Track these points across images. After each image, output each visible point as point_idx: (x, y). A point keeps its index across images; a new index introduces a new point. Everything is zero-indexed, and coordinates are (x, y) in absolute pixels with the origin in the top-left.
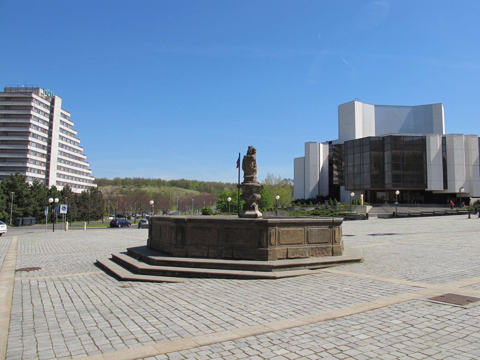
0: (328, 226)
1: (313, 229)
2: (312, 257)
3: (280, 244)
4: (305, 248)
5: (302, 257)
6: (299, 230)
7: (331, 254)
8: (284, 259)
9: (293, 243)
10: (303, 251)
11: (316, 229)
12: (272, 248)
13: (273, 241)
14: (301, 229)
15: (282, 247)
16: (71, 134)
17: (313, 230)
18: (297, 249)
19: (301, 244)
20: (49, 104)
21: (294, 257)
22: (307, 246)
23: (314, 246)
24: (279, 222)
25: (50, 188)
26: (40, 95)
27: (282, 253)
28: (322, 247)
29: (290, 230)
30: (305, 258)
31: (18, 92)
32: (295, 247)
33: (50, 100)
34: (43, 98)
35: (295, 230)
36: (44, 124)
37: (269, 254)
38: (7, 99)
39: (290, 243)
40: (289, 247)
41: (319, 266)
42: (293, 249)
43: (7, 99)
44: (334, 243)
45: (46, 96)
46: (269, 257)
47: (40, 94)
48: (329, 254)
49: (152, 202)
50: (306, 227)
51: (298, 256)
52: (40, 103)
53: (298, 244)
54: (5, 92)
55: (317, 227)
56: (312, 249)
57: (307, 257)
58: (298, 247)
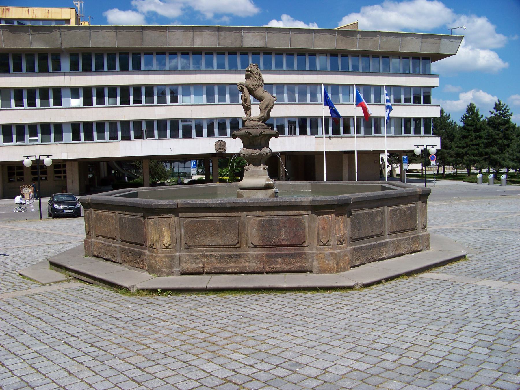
22: (120, 244)
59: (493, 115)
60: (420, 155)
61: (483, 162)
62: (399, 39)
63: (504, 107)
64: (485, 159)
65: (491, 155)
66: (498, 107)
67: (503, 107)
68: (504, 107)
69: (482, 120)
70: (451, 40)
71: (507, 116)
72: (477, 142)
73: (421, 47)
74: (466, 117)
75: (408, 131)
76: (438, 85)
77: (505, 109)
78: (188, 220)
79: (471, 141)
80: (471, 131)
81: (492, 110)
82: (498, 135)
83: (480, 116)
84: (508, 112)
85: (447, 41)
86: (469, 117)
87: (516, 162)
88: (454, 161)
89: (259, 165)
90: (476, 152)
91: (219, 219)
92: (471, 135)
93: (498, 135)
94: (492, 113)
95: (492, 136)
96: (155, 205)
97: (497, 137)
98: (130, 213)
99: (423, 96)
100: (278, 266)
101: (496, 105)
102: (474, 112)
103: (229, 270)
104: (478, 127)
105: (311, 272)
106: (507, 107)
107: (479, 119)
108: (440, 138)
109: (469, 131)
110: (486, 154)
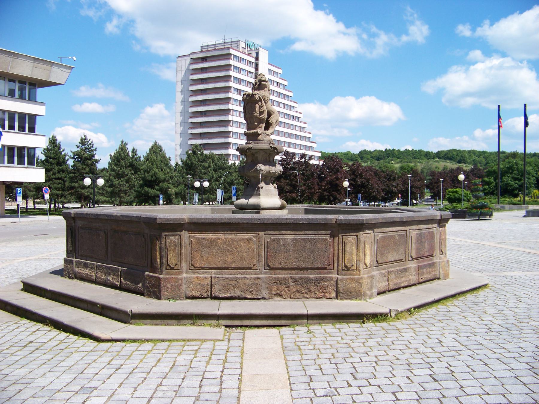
0: (329, 232)
1: (281, 237)
2: (277, 298)
3: (195, 268)
4: (259, 278)
5: (249, 297)
6: (243, 239)
7: (334, 294)
8: (202, 298)
9: (226, 266)
10: (254, 284)
11: (292, 237)
12: (172, 274)
13: (172, 259)
14: (247, 237)
15: (198, 273)
16: (285, 96)
17: (281, 242)
18: (235, 279)
19: (250, 268)
20: (253, 60)
21: (228, 295)
22: (266, 273)
23: (283, 275)
24: (187, 221)
25: (71, 163)
26: (241, 50)
27: (198, 287)
28: (306, 278)
29: (219, 239)
30: (259, 299)
31: (215, 49)
32: (231, 276)
33: (255, 55)
34: (245, 53)
35: (233, 240)
36: (247, 86)
37: (162, 286)
38: (204, 59)
39: (219, 266)
40: (214, 273)
41: (283, 322)
42: (226, 278)
43: (204, 59)
44: (342, 270)
45: (249, 49)
46: (164, 293)
47: (241, 48)
48: (327, 295)
49: (346, 184)
50: (262, 234)
51: (238, 293)
52: (241, 60)
53: (240, 269)
54: (202, 51)
55: (292, 233)
56: (278, 281)
57: (264, 298)
58: (241, 276)
59: (79, 149)
60: (91, 184)
61: (69, 197)
62: (9, 59)
63: (90, 142)
64: (72, 194)
65: (79, 189)
66: (83, 141)
67: (88, 142)
68: (90, 142)
69: (63, 153)
70: (62, 69)
71: (92, 151)
72: (60, 177)
73: (32, 71)
74: (48, 149)
75: (11, 161)
76: (44, 114)
77: (90, 144)
78: (380, 235)
79: (54, 174)
80: (54, 164)
81: (78, 144)
82: (85, 169)
83: (61, 150)
84: (92, 147)
85: (58, 70)
86: (51, 150)
87: (107, 197)
88: (35, 195)
89: (269, 184)
90: (60, 186)
91: (395, 234)
92: (54, 168)
93: (85, 169)
94: (78, 147)
95: (78, 170)
96: (366, 219)
97: (83, 171)
98: (297, 233)
99: (27, 124)
100: (425, 276)
101: (82, 140)
102: (56, 145)
103: (403, 285)
104: (61, 160)
105: (439, 279)
106: (92, 142)
107: (61, 153)
108: (44, 170)
109: (51, 164)
110: (73, 188)
